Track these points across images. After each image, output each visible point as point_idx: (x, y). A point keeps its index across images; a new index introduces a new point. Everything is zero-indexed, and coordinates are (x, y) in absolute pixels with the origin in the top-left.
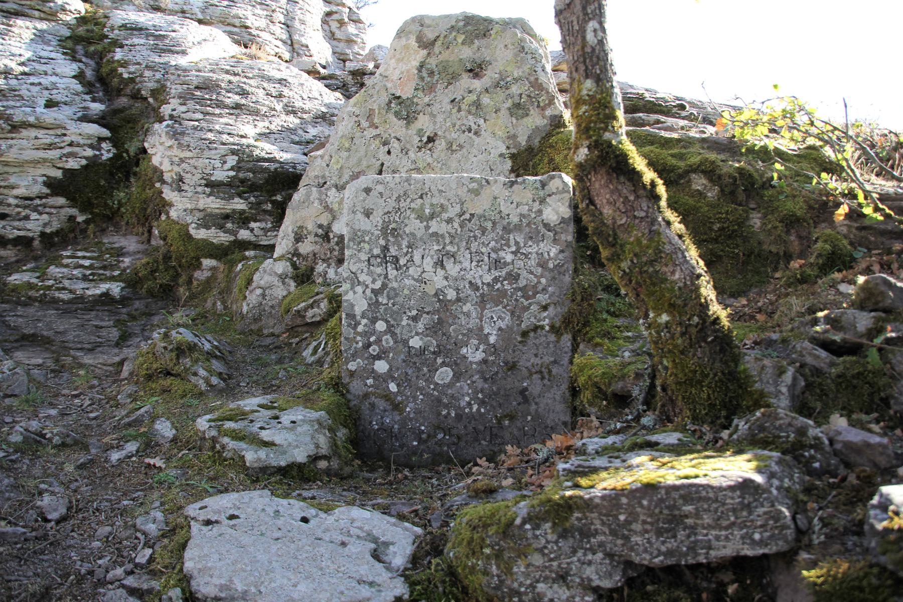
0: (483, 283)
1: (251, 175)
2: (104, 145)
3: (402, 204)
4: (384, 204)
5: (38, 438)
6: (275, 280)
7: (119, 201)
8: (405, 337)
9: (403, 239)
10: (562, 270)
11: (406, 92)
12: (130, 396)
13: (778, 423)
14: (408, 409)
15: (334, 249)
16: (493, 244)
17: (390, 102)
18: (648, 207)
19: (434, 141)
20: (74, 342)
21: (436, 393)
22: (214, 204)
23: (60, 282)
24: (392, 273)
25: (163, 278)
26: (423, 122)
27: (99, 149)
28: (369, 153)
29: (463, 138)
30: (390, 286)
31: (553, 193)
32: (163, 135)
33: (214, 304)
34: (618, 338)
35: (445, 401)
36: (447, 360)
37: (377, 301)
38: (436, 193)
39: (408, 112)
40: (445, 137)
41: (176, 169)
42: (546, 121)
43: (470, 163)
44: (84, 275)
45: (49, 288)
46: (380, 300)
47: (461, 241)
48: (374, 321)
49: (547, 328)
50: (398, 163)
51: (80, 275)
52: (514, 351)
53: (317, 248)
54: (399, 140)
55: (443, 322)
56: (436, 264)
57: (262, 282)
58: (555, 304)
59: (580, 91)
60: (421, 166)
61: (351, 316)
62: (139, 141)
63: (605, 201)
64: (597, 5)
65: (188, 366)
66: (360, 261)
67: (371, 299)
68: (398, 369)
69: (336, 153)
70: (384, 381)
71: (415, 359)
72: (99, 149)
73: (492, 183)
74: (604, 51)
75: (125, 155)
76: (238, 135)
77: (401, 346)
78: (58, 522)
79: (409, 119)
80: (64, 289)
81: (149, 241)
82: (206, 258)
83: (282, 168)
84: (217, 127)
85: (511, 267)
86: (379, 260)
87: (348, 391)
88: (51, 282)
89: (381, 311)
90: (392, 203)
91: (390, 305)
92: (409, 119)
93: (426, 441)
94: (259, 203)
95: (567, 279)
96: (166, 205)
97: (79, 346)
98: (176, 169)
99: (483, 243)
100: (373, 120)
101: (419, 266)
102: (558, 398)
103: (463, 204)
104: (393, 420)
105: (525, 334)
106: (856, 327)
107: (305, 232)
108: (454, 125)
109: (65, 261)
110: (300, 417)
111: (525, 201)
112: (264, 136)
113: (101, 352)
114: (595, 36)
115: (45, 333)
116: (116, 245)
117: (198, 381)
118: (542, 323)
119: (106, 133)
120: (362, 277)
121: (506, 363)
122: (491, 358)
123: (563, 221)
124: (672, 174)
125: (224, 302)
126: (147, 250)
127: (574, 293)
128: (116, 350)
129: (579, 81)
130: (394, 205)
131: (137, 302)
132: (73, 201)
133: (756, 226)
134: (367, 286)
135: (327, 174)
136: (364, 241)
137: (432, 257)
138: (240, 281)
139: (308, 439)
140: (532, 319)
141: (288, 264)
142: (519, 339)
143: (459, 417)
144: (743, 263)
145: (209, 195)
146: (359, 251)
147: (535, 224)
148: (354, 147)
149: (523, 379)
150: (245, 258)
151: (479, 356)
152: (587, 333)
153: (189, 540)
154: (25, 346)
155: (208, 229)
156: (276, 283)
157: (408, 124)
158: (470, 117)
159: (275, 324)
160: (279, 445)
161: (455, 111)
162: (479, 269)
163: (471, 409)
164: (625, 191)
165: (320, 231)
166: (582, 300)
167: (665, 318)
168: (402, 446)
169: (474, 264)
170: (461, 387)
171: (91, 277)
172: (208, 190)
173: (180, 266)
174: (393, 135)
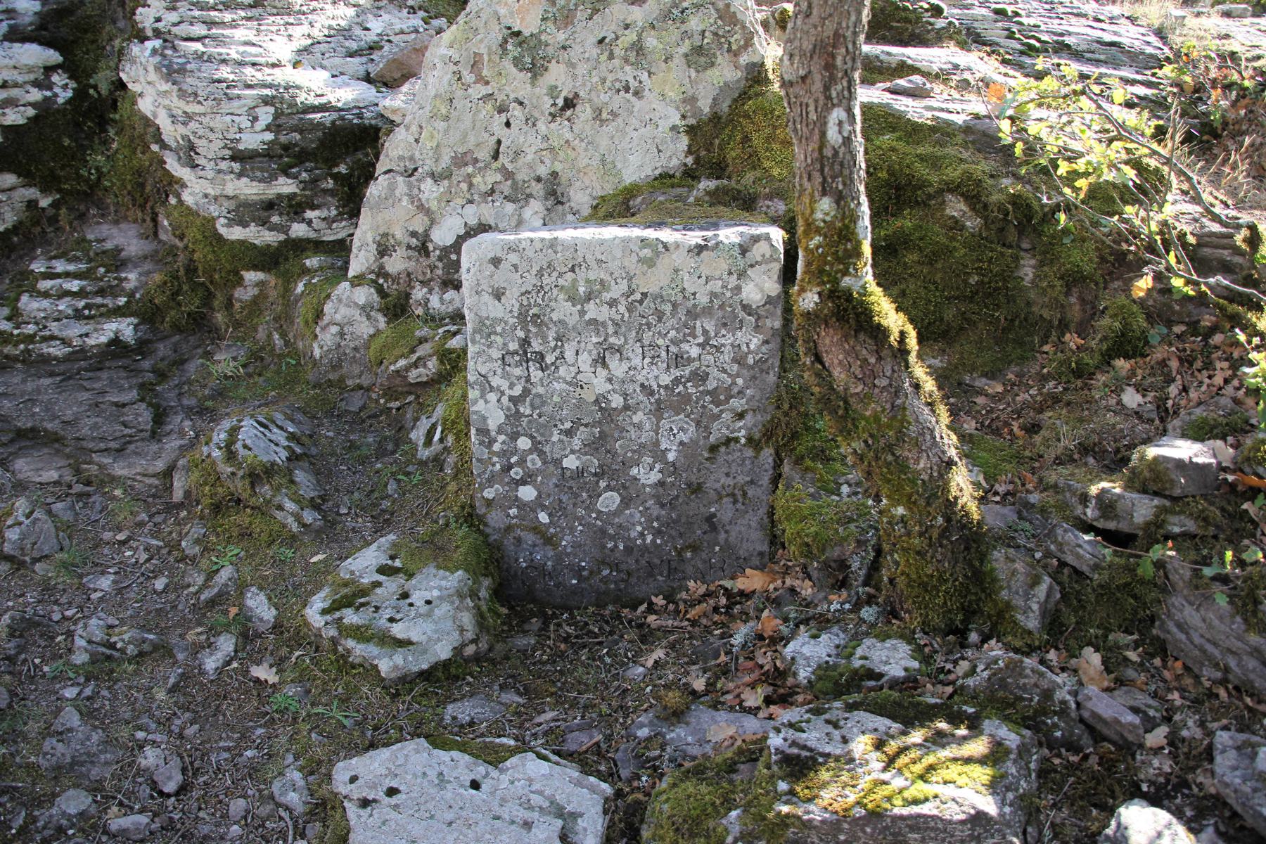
0: (659, 386)
1: (298, 137)
2: (55, 78)
3: (546, 280)
4: (520, 281)
5: (108, 652)
6: (356, 313)
7: (97, 169)
8: (556, 456)
9: (549, 329)
10: (765, 367)
11: (529, 24)
12: (197, 542)
13: (1022, 681)
14: (564, 543)
15: (436, 267)
16: (673, 333)
17: (506, 42)
18: (893, 371)
19: (574, 106)
20: (93, 439)
21: (599, 523)
22: (249, 189)
23: (45, 327)
24: (536, 374)
25: (192, 304)
26: (556, 74)
27: (50, 87)
28: (478, 124)
29: (618, 100)
30: (534, 391)
31: (757, 263)
32: (151, 69)
33: (270, 336)
34: (834, 460)
35: (611, 531)
36: (613, 483)
37: (517, 411)
38: (593, 264)
39: (533, 58)
40: (590, 100)
41: (182, 130)
42: (740, 74)
43: (628, 139)
44: (76, 310)
45: (30, 339)
46: (522, 410)
47: (630, 330)
48: (514, 437)
49: (743, 441)
50: (522, 139)
51: (70, 312)
52: (699, 471)
53: (411, 265)
54: (521, 104)
55: (606, 436)
56: (595, 361)
57: (338, 317)
58: (754, 411)
59: (812, 212)
60: (555, 144)
61: (482, 432)
62: (109, 67)
63: (836, 361)
64: (845, 84)
65: (268, 497)
66: (490, 359)
67: (509, 409)
68: (549, 495)
69: (428, 122)
70: (531, 510)
71: (571, 483)
72: (50, 87)
73: (672, 249)
74: (851, 152)
75: (91, 91)
76: (267, 65)
77: (551, 468)
78: (177, 793)
79: (535, 70)
80: (53, 338)
81: (156, 234)
82: (248, 270)
83: (342, 118)
84: (234, 56)
85: (697, 364)
86: (517, 358)
87: (486, 525)
88: (31, 329)
89: (524, 424)
90: (532, 280)
91: (535, 416)
92: (535, 70)
93: (588, 579)
94: (315, 181)
95: (772, 378)
96: (172, 184)
97: (102, 446)
98: (182, 130)
99: (659, 333)
100: (480, 70)
101: (573, 365)
102: (754, 524)
103: (630, 279)
104: (545, 556)
105: (713, 449)
106: (1132, 517)
107: (392, 241)
108: (603, 81)
109: (44, 285)
110: (436, 593)
111: (717, 274)
112: (303, 56)
113: (137, 454)
114: (840, 132)
115: (49, 426)
116: (109, 245)
117: (286, 518)
118: (736, 434)
119: (53, 56)
120: (496, 381)
121: (689, 485)
122: (669, 480)
123: (770, 301)
124: (919, 193)
125: (283, 335)
126: (156, 252)
127: (779, 398)
128: (154, 447)
129: (812, 196)
130: (534, 282)
131: (161, 346)
132: (28, 177)
133: (1027, 279)
134: (503, 393)
135: (417, 155)
136: (495, 333)
137: (590, 352)
138: (302, 311)
139: (449, 623)
140: (724, 430)
141: (372, 290)
142: (706, 455)
143: (629, 550)
144: (1004, 329)
145: (240, 175)
146: (489, 346)
147: (730, 306)
148: (454, 114)
149: (710, 504)
150: (306, 271)
151: (655, 477)
152: (795, 449)
153: (349, 832)
154: (26, 447)
155: (245, 227)
156: (357, 317)
157: (534, 77)
158: (628, 68)
159: (362, 372)
160: (417, 643)
161: (604, 57)
162: (654, 367)
163: (644, 540)
164: (864, 352)
165: (414, 242)
166: (791, 408)
167: (900, 510)
168: (557, 585)
169: (647, 360)
170: (631, 515)
171: (86, 312)
172: (236, 166)
173: (211, 282)
174: (512, 96)
